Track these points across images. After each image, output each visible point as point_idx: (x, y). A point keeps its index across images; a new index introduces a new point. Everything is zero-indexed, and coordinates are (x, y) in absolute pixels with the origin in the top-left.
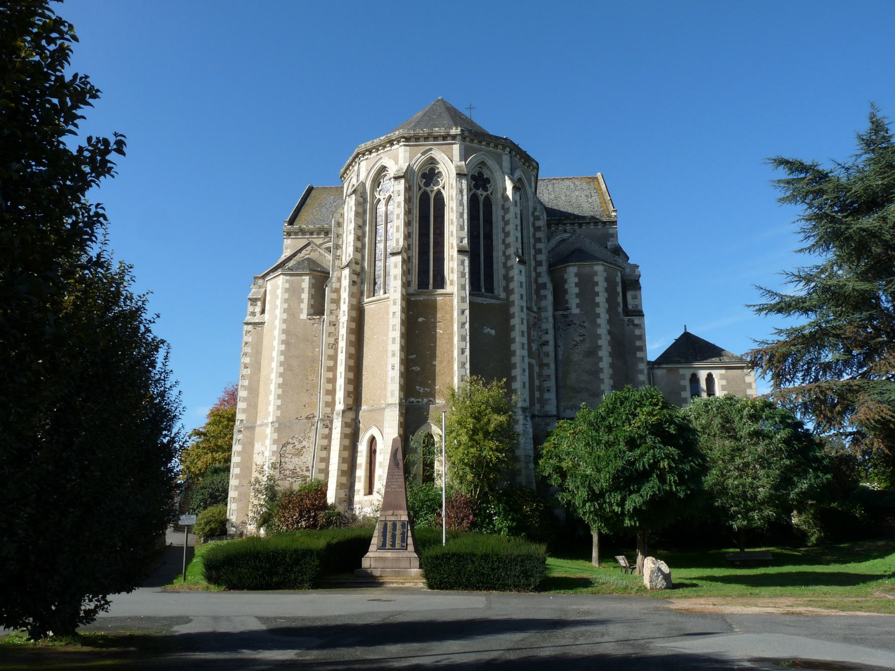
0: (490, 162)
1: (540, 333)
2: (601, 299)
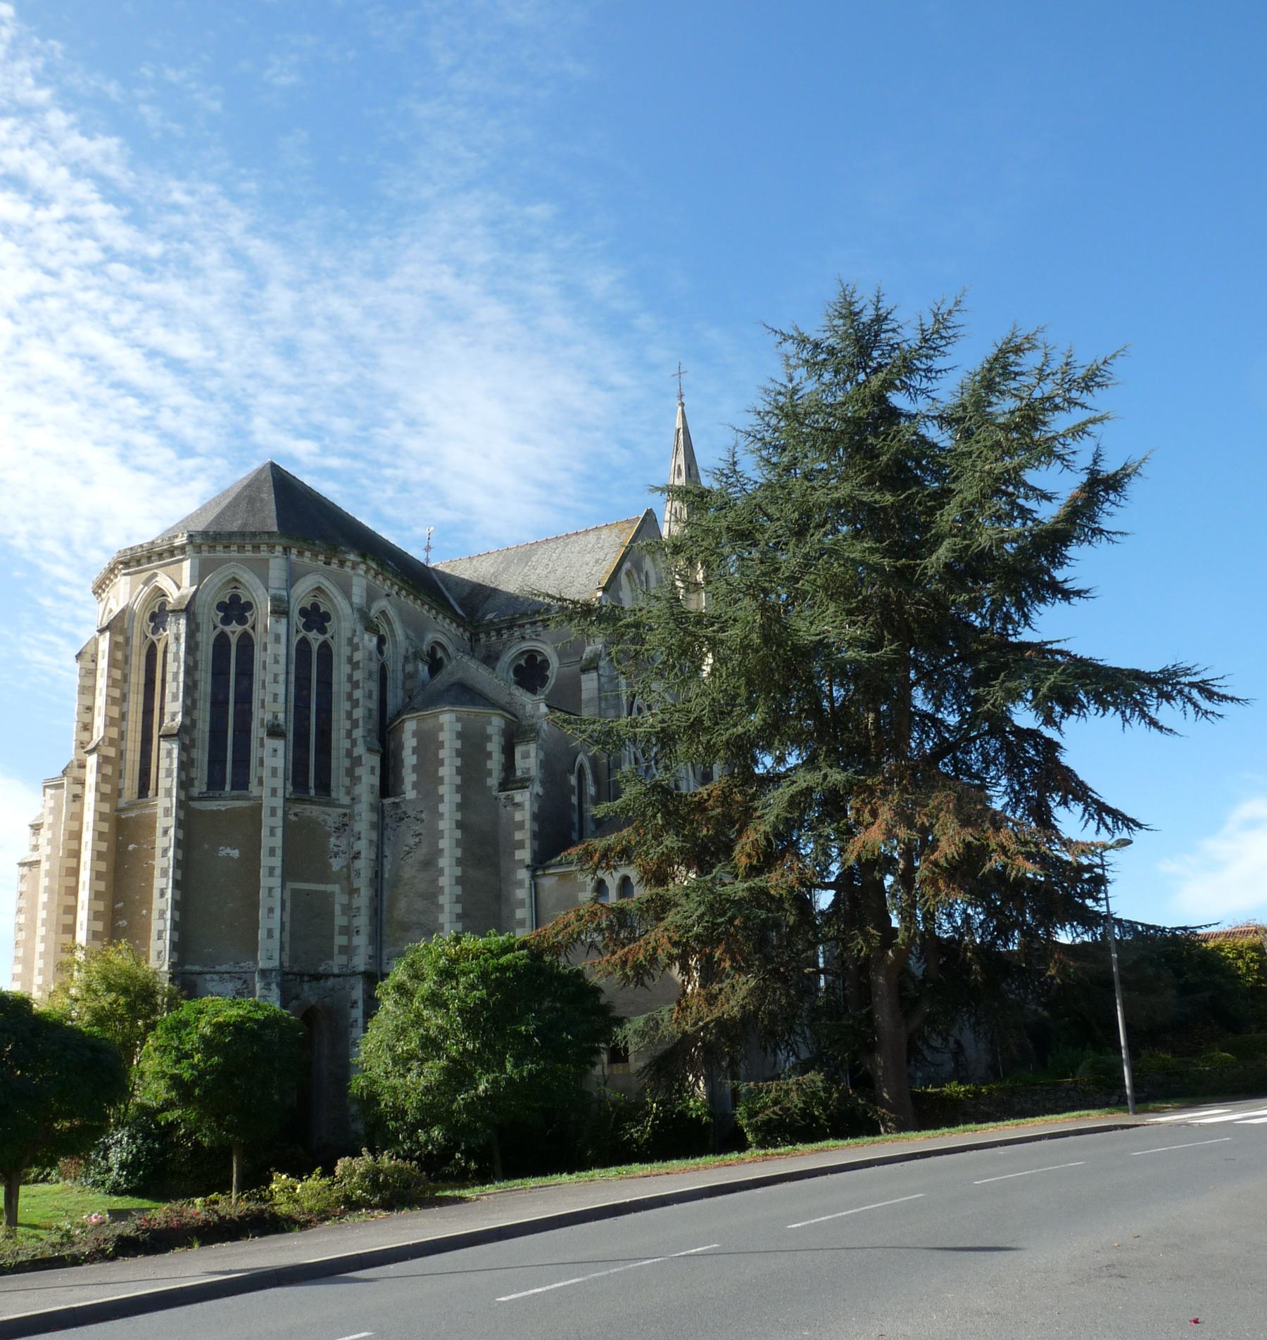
0: (245, 575)
1: (352, 840)
2: (448, 771)
